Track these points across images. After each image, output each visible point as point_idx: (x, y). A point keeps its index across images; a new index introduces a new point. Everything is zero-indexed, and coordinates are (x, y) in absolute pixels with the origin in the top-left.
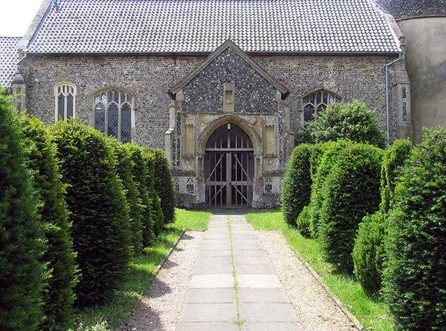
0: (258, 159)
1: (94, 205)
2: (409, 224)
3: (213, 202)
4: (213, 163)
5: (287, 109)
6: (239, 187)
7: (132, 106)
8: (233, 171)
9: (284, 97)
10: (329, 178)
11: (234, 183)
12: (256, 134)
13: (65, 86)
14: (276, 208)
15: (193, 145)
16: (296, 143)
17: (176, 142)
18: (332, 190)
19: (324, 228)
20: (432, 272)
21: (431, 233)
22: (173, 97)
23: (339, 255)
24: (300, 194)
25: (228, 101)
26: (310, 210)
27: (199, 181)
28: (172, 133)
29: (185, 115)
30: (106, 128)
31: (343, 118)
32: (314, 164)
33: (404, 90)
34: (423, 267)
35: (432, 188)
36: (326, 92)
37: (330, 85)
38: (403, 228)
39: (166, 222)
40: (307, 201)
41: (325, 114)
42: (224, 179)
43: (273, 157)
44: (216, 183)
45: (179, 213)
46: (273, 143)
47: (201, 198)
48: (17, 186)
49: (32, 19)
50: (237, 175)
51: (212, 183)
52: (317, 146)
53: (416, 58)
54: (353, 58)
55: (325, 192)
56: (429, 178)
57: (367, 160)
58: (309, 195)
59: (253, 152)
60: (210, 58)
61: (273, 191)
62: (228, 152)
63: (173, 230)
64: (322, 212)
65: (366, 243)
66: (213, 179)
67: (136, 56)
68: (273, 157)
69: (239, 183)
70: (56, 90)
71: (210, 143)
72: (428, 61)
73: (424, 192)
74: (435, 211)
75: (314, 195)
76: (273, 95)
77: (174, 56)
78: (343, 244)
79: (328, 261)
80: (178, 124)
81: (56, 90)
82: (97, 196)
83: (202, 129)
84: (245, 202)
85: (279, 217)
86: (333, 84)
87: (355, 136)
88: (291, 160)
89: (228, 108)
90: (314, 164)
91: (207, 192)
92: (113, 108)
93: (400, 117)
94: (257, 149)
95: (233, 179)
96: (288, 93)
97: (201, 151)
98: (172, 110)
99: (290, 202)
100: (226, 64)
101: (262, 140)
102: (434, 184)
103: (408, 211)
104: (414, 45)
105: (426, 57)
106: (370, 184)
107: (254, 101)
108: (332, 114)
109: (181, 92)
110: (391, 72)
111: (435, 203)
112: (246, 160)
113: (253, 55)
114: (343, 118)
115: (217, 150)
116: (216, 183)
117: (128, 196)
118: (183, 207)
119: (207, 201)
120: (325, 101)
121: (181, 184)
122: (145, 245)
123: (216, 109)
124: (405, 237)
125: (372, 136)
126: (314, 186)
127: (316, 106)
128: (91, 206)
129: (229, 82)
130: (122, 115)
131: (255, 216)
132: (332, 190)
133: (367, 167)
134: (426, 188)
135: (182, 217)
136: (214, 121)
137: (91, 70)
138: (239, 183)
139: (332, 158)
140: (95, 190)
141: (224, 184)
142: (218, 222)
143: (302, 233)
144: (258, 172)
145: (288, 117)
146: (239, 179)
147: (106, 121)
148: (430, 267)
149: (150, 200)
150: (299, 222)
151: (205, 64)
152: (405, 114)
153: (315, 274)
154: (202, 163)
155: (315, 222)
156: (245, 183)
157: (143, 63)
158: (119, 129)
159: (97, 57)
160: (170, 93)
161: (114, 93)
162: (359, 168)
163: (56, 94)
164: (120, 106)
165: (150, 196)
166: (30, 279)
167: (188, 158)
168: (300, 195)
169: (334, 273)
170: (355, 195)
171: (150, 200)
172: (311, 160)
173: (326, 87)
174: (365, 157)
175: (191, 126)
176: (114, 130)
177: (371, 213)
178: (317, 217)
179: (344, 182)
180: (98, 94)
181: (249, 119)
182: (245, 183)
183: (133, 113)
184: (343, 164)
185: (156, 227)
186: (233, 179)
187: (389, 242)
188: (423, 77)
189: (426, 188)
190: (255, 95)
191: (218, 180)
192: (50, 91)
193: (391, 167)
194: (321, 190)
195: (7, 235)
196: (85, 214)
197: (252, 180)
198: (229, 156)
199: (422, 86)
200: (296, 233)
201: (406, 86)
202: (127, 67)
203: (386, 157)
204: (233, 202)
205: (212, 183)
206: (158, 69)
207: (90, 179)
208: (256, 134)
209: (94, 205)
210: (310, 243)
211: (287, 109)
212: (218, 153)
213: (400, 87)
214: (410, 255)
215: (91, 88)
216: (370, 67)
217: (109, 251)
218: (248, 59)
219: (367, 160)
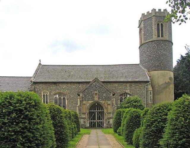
0: (105, 114)
1: (59, 127)
2: (147, 130)
3: (92, 126)
4: (91, 115)
5: (114, 99)
6: (100, 122)
7: (66, 98)
8: (98, 117)
9: (113, 95)
10: (126, 119)
11: (98, 121)
12: (105, 106)
13: (45, 91)
14: (111, 128)
15: (86, 109)
16: (117, 109)
17: (80, 109)
18: (127, 122)
19: (125, 133)
20: (153, 142)
21: (152, 132)
22: (79, 95)
23: (129, 139)
24: (118, 124)
25: (96, 97)
26: (121, 128)
27: (87, 120)
28: (79, 106)
29: (83, 101)
30: (58, 104)
31: (132, 101)
32: (122, 115)
33: (151, 92)
34: (150, 141)
35: (153, 121)
36: (127, 94)
37: (128, 91)
38: (145, 131)
39: (78, 132)
40: (120, 126)
41: (126, 100)
42: (95, 120)
43: (110, 113)
44: (92, 121)
45: (81, 129)
46: (110, 109)
47: (88, 125)
48: (44, 121)
49: (35, 71)
50: (99, 118)
51: (91, 121)
52: (123, 110)
53: (154, 83)
54: (135, 83)
55: (125, 123)
56: (153, 118)
57: (137, 114)
58: (121, 124)
59: (104, 112)
60: (90, 83)
61: (110, 123)
62: (96, 112)
63: (79, 134)
64: (124, 128)
65: (136, 136)
66: (91, 120)
67: (67, 83)
68: (110, 113)
69: (100, 121)
70: (42, 93)
71: (90, 109)
72: (158, 83)
73: (151, 122)
74: (153, 127)
75: (122, 124)
76: (110, 95)
77: (79, 83)
78: (130, 137)
79: (126, 142)
80: (80, 103)
81: (42, 93)
82: (60, 124)
83: (88, 105)
84: (101, 126)
85: (112, 130)
86: (129, 91)
87: (135, 107)
88: (115, 114)
89: (96, 99)
90: (122, 115)
91: (90, 123)
92: (60, 99)
93: (149, 100)
94: (105, 111)
95: (98, 120)
96: (115, 94)
97: (88, 111)
98: (79, 99)
99: (115, 126)
100: (95, 85)
101: (107, 108)
102: (153, 120)
103: (147, 127)
104: (154, 79)
105: (186, 54)
106: (138, 120)
107: (104, 97)
108: (128, 100)
109: (81, 94)
110: (147, 87)
111: (153, 125)
112: (101, 115)
113: (103, 82)
114: (132, 101)
115: (92, 111)
116: (92, 121)
117: (68, 124)
118: (82, 128)
119: (90, 126)
120: (126, 96)
121: (82, 121)
122: (73, 138)
123: (93, 98)
124: (145, 134)
125: (141, 107)
126: (122, 121)
127: (123, 98)
128: (58, 127)
129: (96, 91)
130: (63, 102)
131: (105, 130)
132: (127, 122)
133: (137, 115)
134: (151, 121)
135: (82, 130)
136: (92, 103)
137: (53, 87)
138: (100, 121)
139: (128, 113)
140: (59, 123)
141: (95, 121)
142: (93, 131)
143: (119, 135)
144: (105, 117)
145: (115, 101)
146: (100, 120)
147: (58, 103)
148: (152, 141)
149: (74, 126)
150: (118, 131)
151: (89, 85)
152: (151, 99)
153: (122, 145)
154: (88, 115)
155: (122, 131)
156: (101, 121)
157: (69, 85)
158: (62, 105)
159: (55, 83)
160: (78, 94)
161: (60, 94)
162: (135, 116)
163: (43, 94)
164: (62, 98)
165: (73, 124)
166: (48, 144)
167: (84, 114)
168: (118, 124)
169: (128, 144)
170: (134, 123)
171: (74, 126)
172: (121, 114)
173: (127, 92)
174: (137, 112)
175: (85, 104)
176: (60, 105)
177: (138, 128)
178: (123, 130)
179: (131, 120)
180: (55, 94)
181: (102, 102)
182: (101, 121)
183: (66, 100)
184: (130, 115)
185: (76, 132)
186: (98, 120)
187: (142, 135)
188: (157, 88)
189: (151, 121)
190: (105, 95)
191: (93, 120)
192: (41, 93)
193: (143, 115)
194: (124, 122)
195: (42, 133)
196: (57, 129)
197: (103, 119)
198: (96, 113)
199: (156, 91)
200: (117, 135)
201: (151, 91)
202: (64, 86)
203: (142, 113)
204: (98, 126)
205: (91, 121)
206: (74, 87)
207: (58, 120)
208: (105, 106)
209: (59, 127)
210: (121, 137)
211: (114, 99)
212: (93, 112)
213: (149, 91)
214: (147, 138)
215: (53, 92)
216: (140, 86)
217: (63, 139)
218: (102, 84)
219: (137, 114)
